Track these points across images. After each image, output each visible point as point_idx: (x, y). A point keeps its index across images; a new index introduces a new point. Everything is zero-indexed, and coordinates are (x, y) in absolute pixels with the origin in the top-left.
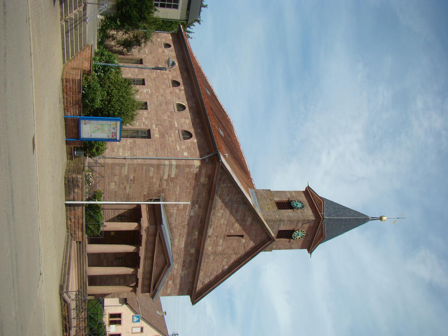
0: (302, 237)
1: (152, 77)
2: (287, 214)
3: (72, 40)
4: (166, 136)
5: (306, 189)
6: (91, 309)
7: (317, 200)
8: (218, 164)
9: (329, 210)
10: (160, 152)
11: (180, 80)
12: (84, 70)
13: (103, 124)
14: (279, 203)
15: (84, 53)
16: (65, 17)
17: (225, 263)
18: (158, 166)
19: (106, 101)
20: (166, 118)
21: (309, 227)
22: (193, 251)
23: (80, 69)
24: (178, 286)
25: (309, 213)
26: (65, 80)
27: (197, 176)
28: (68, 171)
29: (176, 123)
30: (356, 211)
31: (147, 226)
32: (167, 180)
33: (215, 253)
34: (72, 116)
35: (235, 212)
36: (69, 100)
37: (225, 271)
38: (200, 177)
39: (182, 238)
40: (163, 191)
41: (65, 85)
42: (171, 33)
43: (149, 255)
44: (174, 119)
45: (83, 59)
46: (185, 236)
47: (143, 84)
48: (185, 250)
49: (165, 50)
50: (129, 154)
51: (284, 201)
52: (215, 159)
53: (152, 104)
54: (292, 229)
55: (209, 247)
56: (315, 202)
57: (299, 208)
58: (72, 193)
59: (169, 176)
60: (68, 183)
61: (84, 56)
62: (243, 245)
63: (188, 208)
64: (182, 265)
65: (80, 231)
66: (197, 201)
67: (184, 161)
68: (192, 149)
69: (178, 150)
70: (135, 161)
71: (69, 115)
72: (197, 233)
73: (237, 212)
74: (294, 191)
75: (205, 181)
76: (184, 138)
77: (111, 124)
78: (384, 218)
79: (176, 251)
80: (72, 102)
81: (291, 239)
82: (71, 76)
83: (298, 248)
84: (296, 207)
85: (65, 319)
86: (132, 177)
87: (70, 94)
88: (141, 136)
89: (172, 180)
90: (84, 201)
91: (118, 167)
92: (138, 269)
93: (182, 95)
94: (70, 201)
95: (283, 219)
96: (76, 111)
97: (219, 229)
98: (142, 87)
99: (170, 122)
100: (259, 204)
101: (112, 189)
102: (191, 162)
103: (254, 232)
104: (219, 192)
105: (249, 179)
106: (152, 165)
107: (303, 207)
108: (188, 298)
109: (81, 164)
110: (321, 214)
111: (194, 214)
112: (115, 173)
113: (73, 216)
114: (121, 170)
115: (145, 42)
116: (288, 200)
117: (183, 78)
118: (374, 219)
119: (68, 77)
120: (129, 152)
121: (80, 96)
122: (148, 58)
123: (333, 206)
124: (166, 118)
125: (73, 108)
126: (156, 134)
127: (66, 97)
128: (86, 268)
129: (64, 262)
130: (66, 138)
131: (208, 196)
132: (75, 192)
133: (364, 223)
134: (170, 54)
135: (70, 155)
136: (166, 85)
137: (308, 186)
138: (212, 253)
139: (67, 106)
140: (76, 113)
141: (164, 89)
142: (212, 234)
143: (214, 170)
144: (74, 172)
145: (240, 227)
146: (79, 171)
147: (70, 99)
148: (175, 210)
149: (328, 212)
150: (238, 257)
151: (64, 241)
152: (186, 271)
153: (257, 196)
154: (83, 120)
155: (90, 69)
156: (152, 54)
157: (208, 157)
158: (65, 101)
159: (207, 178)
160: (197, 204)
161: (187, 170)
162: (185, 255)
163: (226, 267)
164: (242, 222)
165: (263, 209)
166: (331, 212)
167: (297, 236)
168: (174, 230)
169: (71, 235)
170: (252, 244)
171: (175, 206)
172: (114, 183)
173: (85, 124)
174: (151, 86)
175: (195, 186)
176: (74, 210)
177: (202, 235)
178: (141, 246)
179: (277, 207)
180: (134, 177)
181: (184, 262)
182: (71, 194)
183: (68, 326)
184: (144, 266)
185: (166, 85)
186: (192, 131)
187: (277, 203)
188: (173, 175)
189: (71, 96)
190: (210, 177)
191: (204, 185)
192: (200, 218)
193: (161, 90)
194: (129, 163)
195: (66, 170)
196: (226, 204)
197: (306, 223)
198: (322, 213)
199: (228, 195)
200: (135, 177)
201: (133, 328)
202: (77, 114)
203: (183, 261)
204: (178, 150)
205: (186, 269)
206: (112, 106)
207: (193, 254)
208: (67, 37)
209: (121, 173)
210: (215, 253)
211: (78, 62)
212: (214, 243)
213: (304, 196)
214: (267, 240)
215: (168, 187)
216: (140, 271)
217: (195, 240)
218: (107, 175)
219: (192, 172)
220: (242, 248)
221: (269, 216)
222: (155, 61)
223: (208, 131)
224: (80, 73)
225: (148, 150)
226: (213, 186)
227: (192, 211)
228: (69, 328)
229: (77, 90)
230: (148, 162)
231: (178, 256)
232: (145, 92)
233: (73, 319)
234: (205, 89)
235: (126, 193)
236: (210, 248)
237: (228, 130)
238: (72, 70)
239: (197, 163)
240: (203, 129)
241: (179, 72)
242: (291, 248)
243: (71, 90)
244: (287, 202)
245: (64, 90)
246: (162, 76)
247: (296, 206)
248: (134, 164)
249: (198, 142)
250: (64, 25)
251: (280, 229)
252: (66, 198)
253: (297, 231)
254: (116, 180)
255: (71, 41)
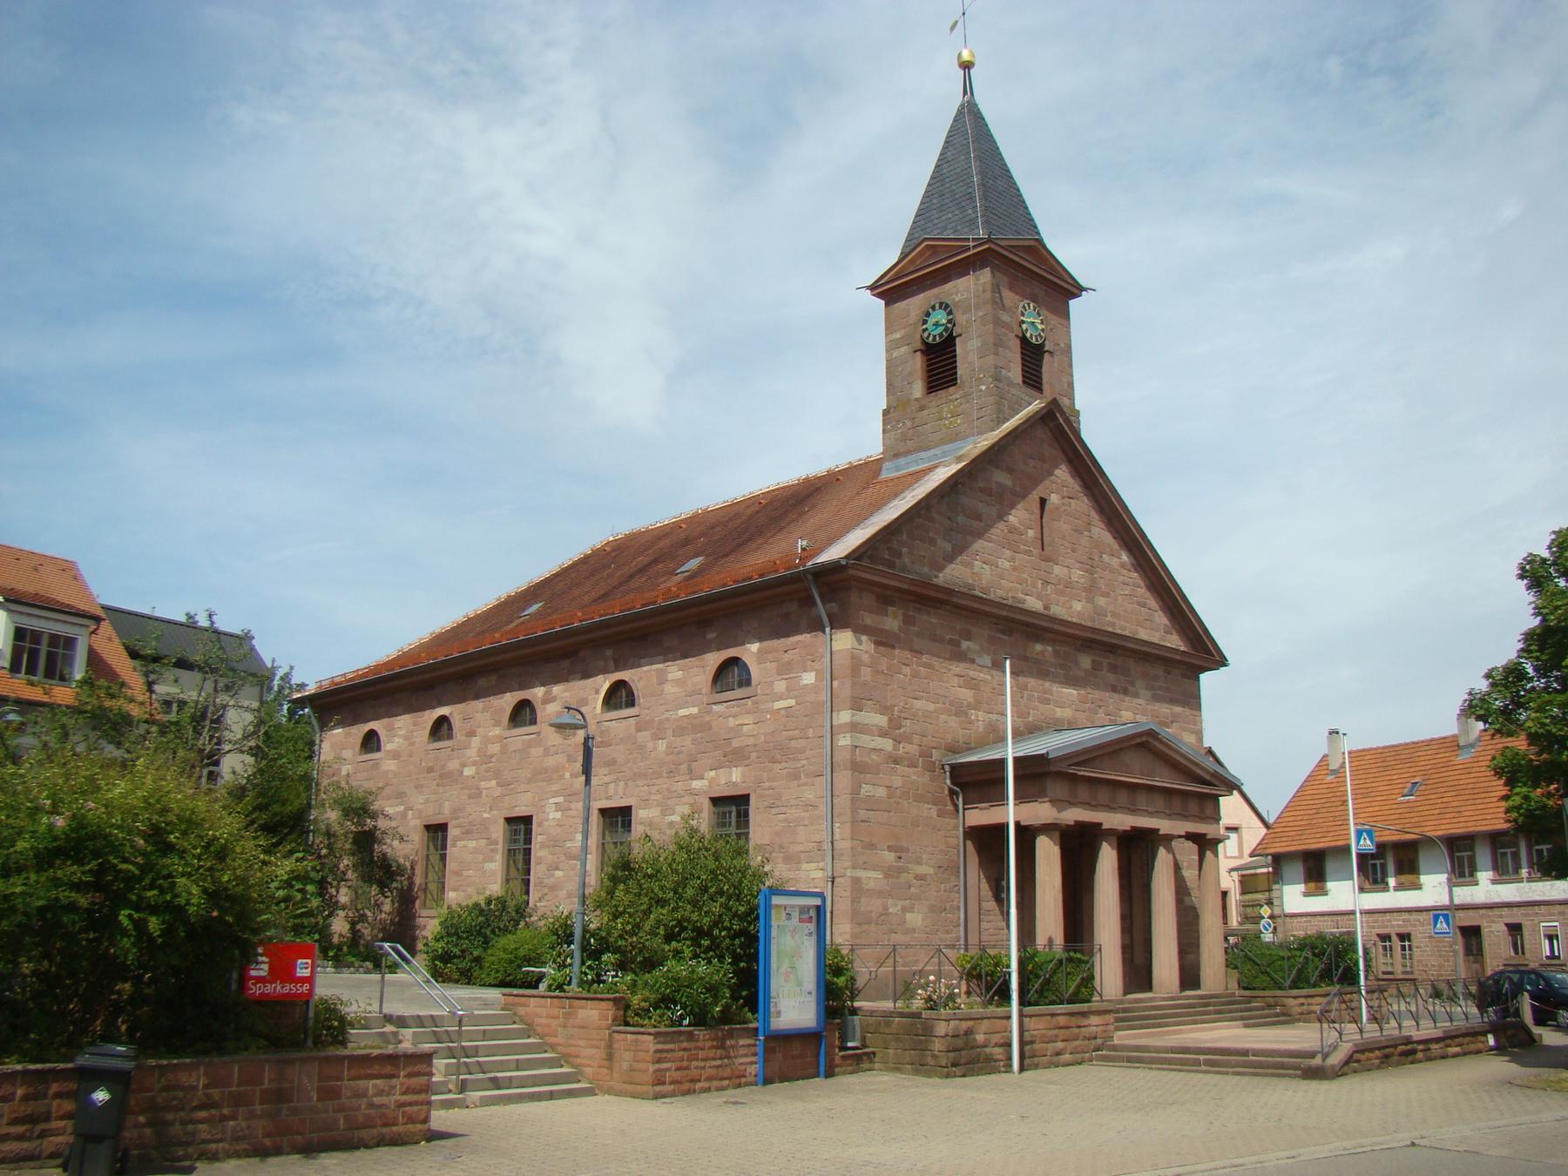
0: (1039, 315)
1: (498, 791)
2: (973, 357)
3: (514, 1066)
4: (736, 743)
5: (879, 295)
6: (1272, 979)
7: (918, 262)
8: (851, 572)
9: (953, 225)
10: (805, 762)
11: (509, 700)
12: (614, 1020)
13: (779, 952)
14: (929, 383)
15: (543, 1021)
16: (450, 1091)
17: (1116, 559)
18: (857, 768)
19: (700, 946)
20: (662, 745)
21: (1011, 288)
22: (1085, 661)
23: (610, 1035)
24: (1178, 709)
25: (969, 289)
26: (659, 1088)
27: (884, 641)
28: (922, 1066)
29: (682, 712)
30: (946, 142)
31: (1047, 805)
32: (897, 741)
33: (1091, 590)
34: (760, 1058)
35: (978, 522)
36: (713, 1072)
37: (1134, 561)
38: (886, 630)
39: (1052, 694)
40: (926, 754)
41: (672, 1087)
42: (322, 731)
43: (1123, 797)
44: (667, 719)
45: (565, 1026)
46: (1047, 684)
47: (527, 820)
48: (1084, 687)
49: (389, 751)
50: (813, 865)
51: (925, 366)
52: (832, 579)
53: (607, 793)
54: (1018, 342)
55: (1074, 610)
56: (930, 265)
57: (951, 317)
58: (988, 1050)
59: (883, 734)
60: (960, 1065)
61: (555, 1022)
62: (1066, 500)
63: (971, 673)
64: (1122, 696)
65: (1086, 1022)
66: (952, 642)
67: (835, 683)
68: (786, 657)
69: (792, 702)
70: (843, 845)
71: (752, 1069)
72: (1039, 647)
73: (978, 517)
74: (886, 335)
75: (895, 616)
76: (740, 686)
77: (778, 926)
78: (966, 56)
79: (1087, 713)
80: (718, 1062)
81: (1046, 349)
82: (643, 1066)
83: (1068, 327)
84: (946, 329)
85: (1387, 1056)
86: (890, 857)
87: (696, 1068)
88: (525, 844)
89: (895, 723)
90: (1010, 1012)
91: (863, 900)
92: (1161, 833)
93: (567, 694)
94: (1010, 1058)
95: (992, 370)
96: (743, 1046)
97: (1025, 576)
98: (540, 824)
99: (680, 731)
100: (937, 446)
101: (923, 920)
102: (842, 662)
103: (1031, 462)
104: (926, 570)
105: (838, 480)
106: (855, 791)
107: (944, 306)
108: (1206, 679)
109: (888, 1024)
110: (974, 247)
111: (989, 654)
112: (881, 910)
113: (1050, 1046)
114: (870, 893)
115: (374, 816)
116: (919, 354)
117: (499, 690)
118: (968, 88)
119: (649, 1078)
120: (804, 866)
121: (701, 1033)
122: (420, 807)
123: (934, 212)
124: (662, 745)
125: (735, 1057)
126: (733, 779)
127: (705, 1080)
128: (1163, 999)
129: (1203, 1068)
130: (817, 1075)
131: (939, 608)
132: (986, 1040)
133: (983, 119)
134: (402, 732)
135: (860, 1060)
136: (530, 745)
137: (868, 288)
138: (1090, 600)
139: (730, 1078)
140: (749, 1045)
141: (546, 753)
142: (1039, 597)
143: (869, 585)
144: (921, 1047)
145: (1019, 506)
146: (920, 1032)
147: (710, 1067)
148: (977, 716)
149: (959, 228)
150: (1096, 517)
151: (1165, 1073)
152: (1139, 684)
153: (908, 453)
154: (769, 1022)
155: (608, 999)
156: (405, 793)
157: (824, 603)
158: (715, 1083)
159: (887, 611)
160: (960, 643)
161: (866, 674)
162: (1097, 686)
163: (1125, 557)
164: (1005, 501)
165: (957, 435)
166: (956, 218)
167: (1036, 328)
168: (1031, 719)
169: (1097, 1049)
170: (1062, 473)
171: (967, 714)
172: (909, 916)
173: (779, 1013)
174: (534, 797)
175: (911, 650)
176: (1032, 1042)
177: (1046, 629)
178: (1101, 824)
179: (948, 387)
180: (890, 849)
181: (1114, 689)
182: (991, 1054)
183: (1403, 1047)
184: (1152, 813)
185: (530, 746)
186: (714, 659)
187: (929, 388)
188: (881, 721)
189: (702, 1064)
190: (887, 598)
191: (908, 620)
192: (1000, 635)
193: (550, 762)
194: (848, 864)
195: (917, 1072)
196: (959, 550)
197: (1001, 296)
198: (971, 244)
199: (933, 542)
200: (888, 847)
201: (1228, 855)
202: (751, 1041)
203: (1113, 694)
204: (792, 702)
205: (1133, 684)
206: (715, 924)
207: (1093, 661)
208: (509, 1083)
209: (880, 892)
210: (1091, 590)
211: (582, 1043)
212: (1062, 593)
213: (906, 302)
214: (1051, 425)
215: (916, 739)
216: (1164, 826)
217: (1056, 654)
218: (886, 936)
219: (872, 656)
220: (1073, 505)
221: (983, 414)
222: (435, 783)
223: (738, 600)
224: (629, 1036)
225: (793, 802)
226: (912, 588)
227: (978, 660)
228: (1406, 1044)
229: (685, 1045)
230: (843, 801)
231: (1100, 707)
232: (558, 815)
233: (1365, 1036)
234: (523, 623)
235: (936, 874)
236: (1078, 606)
237: (661, 545)
238: (616, 1065)
239: (844, 640)
240: (705, 622)
241: (478, 705)
242: (1068, 350)
243: (685, 1064)
244: (925, 358)
245: (687, 1088)
246: (494, 759)
247: (940, 329)
248: (852, 848)
249: (761, 640)
250: (482, 1097)
251: (1019, 380)
252: (1003, 1069)
253: (1024, 326)
254: (899, 907)
255: (517, 1069)
